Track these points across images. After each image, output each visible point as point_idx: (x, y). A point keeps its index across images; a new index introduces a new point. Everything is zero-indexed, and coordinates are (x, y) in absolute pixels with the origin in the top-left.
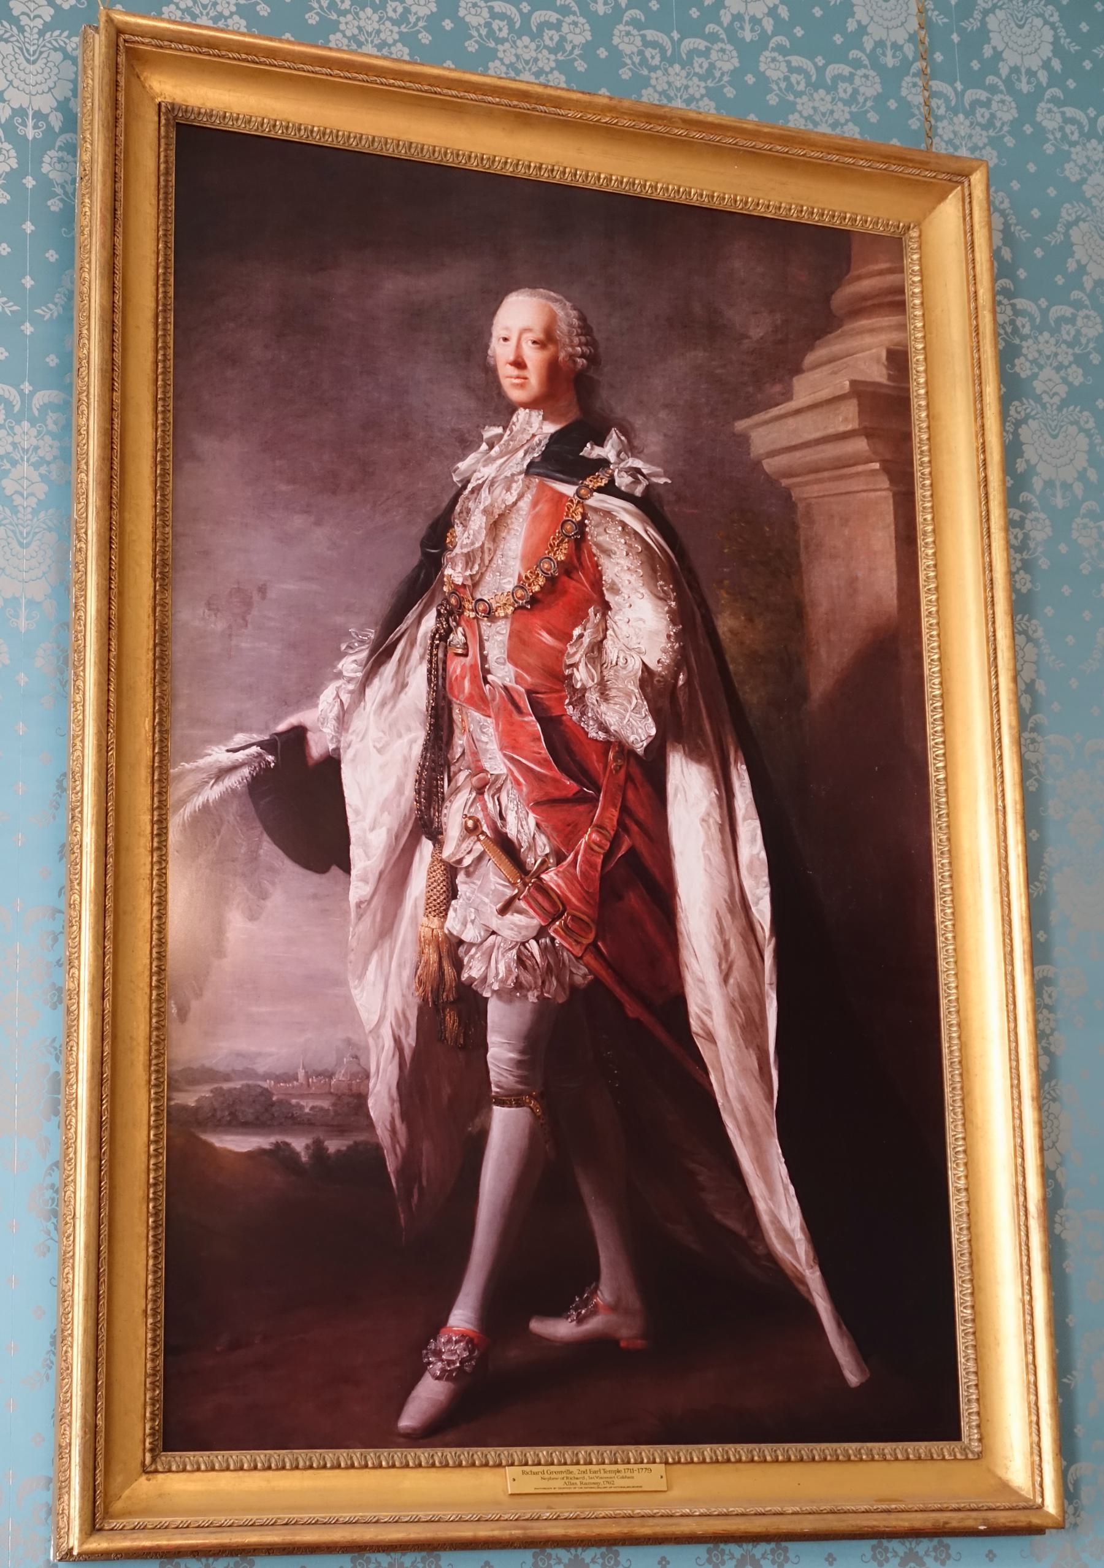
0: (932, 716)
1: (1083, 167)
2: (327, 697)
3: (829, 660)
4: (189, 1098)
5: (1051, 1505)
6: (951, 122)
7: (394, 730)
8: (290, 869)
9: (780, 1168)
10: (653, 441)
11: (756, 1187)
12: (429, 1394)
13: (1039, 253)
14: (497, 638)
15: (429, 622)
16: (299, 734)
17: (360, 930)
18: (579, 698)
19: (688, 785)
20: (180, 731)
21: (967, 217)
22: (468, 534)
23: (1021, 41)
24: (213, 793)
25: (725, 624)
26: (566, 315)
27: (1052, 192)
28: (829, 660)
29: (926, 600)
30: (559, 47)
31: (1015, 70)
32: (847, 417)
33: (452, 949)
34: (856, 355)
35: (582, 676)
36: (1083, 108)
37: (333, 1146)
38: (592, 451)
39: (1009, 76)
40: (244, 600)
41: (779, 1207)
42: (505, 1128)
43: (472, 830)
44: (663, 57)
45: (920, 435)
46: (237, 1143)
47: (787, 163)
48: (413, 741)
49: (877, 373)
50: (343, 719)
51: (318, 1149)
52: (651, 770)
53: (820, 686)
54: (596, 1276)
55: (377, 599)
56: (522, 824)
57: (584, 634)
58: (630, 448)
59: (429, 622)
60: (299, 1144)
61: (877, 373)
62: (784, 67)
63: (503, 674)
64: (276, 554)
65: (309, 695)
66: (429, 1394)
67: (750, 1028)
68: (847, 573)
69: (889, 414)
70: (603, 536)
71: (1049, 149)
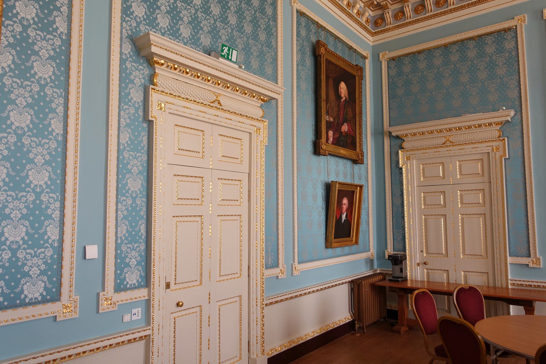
1: (57, 104)
6: (58, 99)
13: (136, 142)
23: (43, 70)
27: (24, 161)
30: (31, 91)
31: (135, 102)
39: (38, 79)
44: (58, 96)
62: (52, 91)
71: (125, 162)
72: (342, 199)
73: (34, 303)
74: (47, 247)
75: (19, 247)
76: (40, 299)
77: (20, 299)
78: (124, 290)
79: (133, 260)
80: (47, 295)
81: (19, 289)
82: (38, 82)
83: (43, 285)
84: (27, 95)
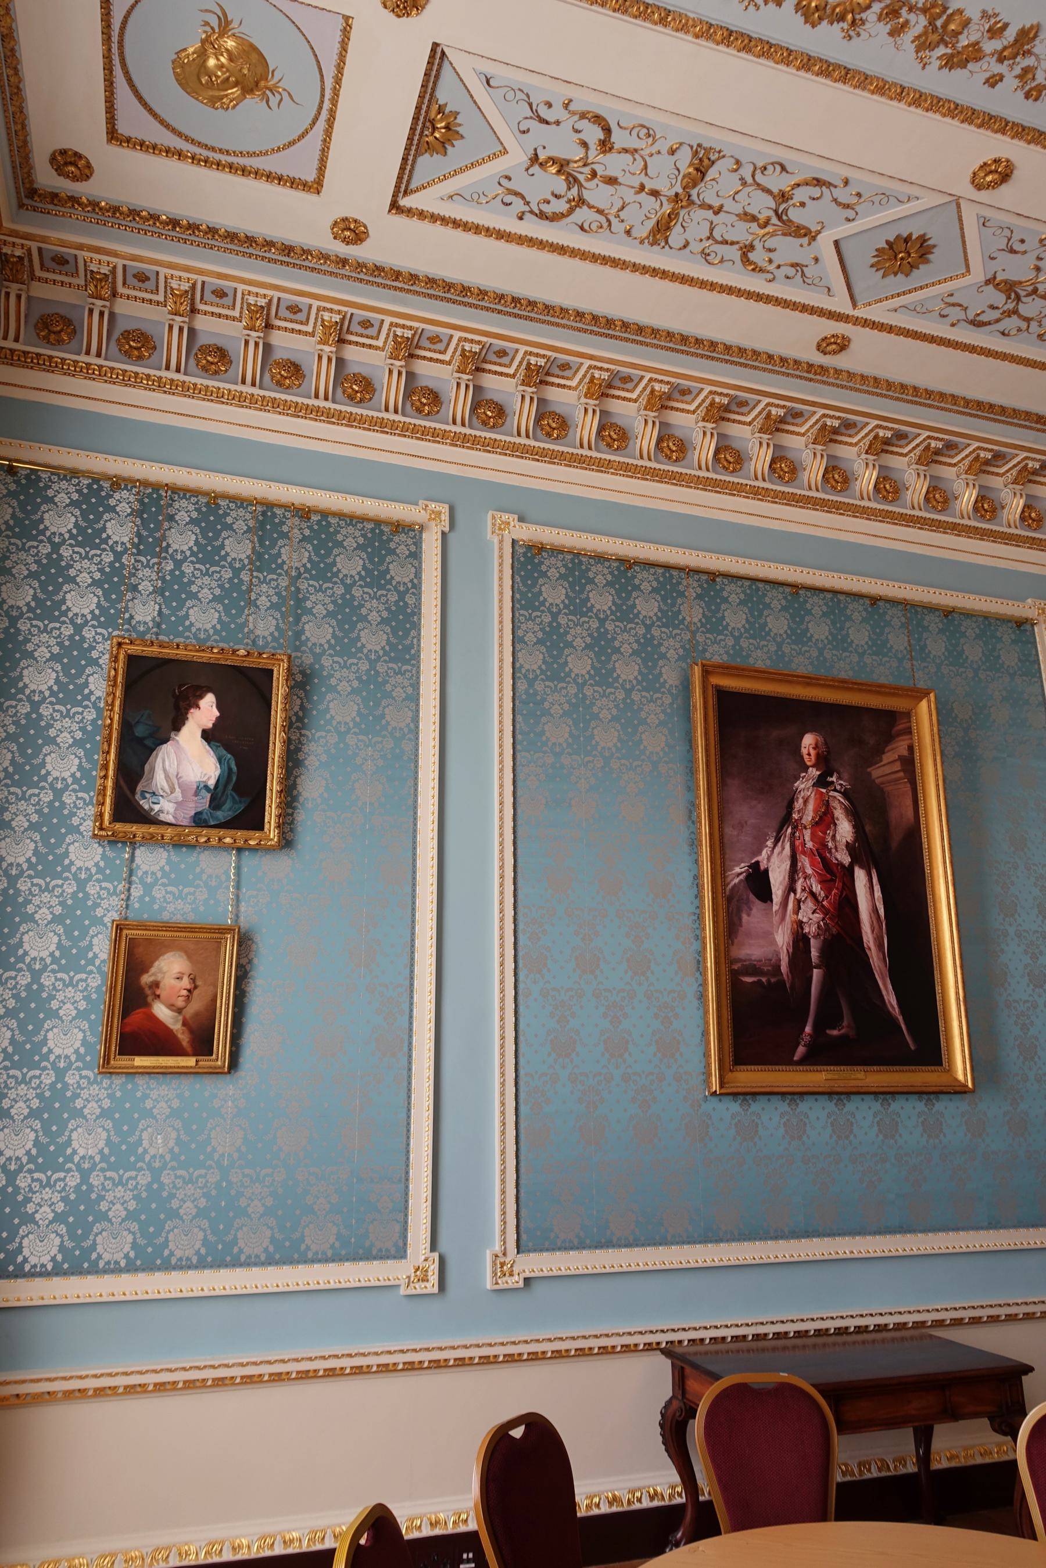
0: (926, 854)
2: (764, 852)
3: (896, 837)
4: (735, 967)
5: (970, 1085)
7: (782, 861)
8: (757, 902)
9: (890, 987)
10: (846, 775)
11: (884, 993)
12: (801, 1050)
14: (807, 834)
15: (789, 830)
16: (758, 862)
17: (776, 919)
18: (830, 852)
19: (860, 876)
20: (728, 863)
21: (929, 707)
22: (798, 804)
24: (736, 881)
25: (868, 828)
26: (820, 739)
28: (896, 837)
29: (922, 820)
32: (897, 766)
33: (800, 924)
34: (900, 747)
35: (830, 844)
36: (20, 788)
37: (773, 980)
38: (830, 779)
40: (741, 825)
41: (891, 998)
42: (816, 973)
43: (804, 890)
45: (918, 771)
46: (749, 979)
47: (879, 693)
48: (787, 865)
49: (905, 753)
50: (769, 859)
51: (769, 981)
52: (848, 873)
53: (894, 845)
54: (842, 1018)
55: (775, 824)
56: (816, 888)
57: (830, 832)
58: (839, 778)
59: (789, 830)
60: (764, 980)
61: (905, 753)
63: (809, 844)
64: (748, 812)
65: (760, 853)
66: (801, 1050)
67: (880, 946)
68: (900, 811)
69: (909, 765)
70: (835, 804)
71: (233, 1192)
72: (189, 957)
73: (114, 1269)
74: (141, 1169)
75: (20, 1169)
76: (49, 1267)
77: (89, 1260)
78: (211, 1267)
79: (46, 1208)
80: (63, 1262)
81: (162, 1240)
82: (49, 540)
83: (57, 1241)
84: (537, 628)
